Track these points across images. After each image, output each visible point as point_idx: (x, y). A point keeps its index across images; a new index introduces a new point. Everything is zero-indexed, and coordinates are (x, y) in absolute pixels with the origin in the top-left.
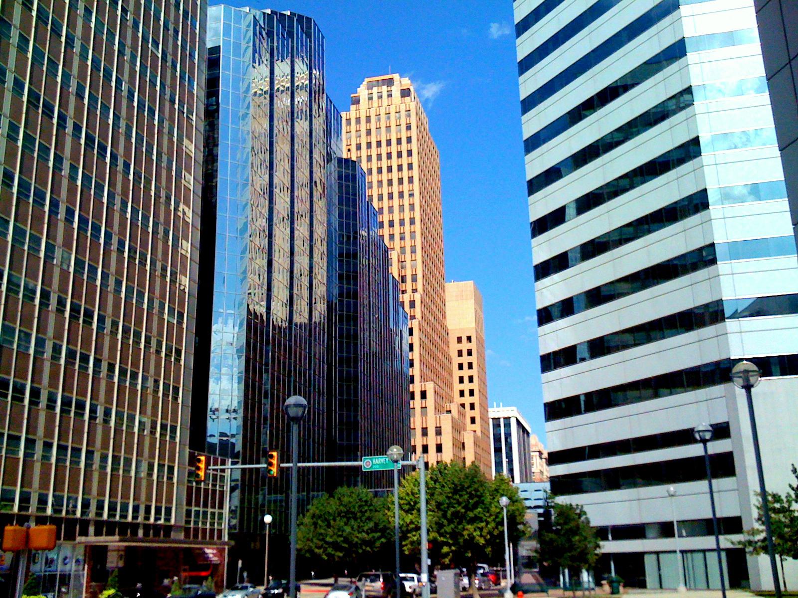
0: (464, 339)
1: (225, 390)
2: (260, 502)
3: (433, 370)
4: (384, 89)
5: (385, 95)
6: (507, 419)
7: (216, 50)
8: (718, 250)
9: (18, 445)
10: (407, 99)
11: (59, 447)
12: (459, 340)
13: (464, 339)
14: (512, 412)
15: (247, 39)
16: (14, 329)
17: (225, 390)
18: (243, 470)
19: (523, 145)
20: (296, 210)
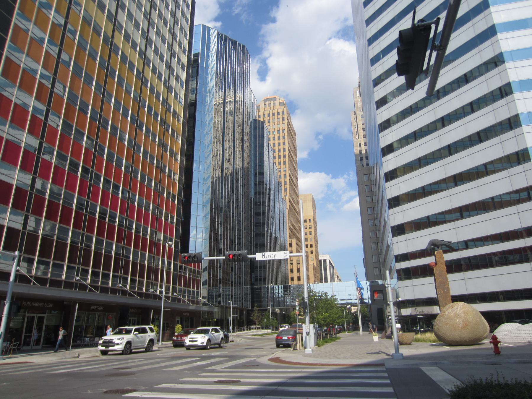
0: (308, 221)
1: (199, 240)
2: (221, 285)
3: (295, 235)
4: (272, 102)
5: (272, 104)
6: (325, 261)
7: (197, 55)
8: (513, 86)
9: (49, 265)
10: (283, 107)
11: (93, 273)
12: (305, 221)
13: (308, 221)
14: (327, 257)
15: (209, 149)
16: (136, 280)
17: (199, 240)
18: (210, 261)
19: (369, 61)
20: (235, 144)
